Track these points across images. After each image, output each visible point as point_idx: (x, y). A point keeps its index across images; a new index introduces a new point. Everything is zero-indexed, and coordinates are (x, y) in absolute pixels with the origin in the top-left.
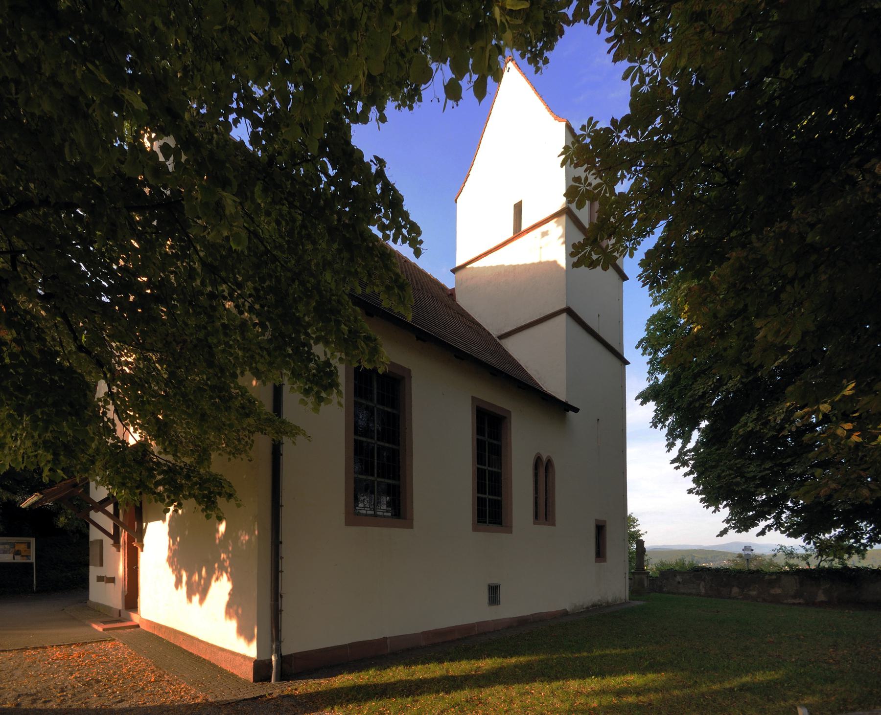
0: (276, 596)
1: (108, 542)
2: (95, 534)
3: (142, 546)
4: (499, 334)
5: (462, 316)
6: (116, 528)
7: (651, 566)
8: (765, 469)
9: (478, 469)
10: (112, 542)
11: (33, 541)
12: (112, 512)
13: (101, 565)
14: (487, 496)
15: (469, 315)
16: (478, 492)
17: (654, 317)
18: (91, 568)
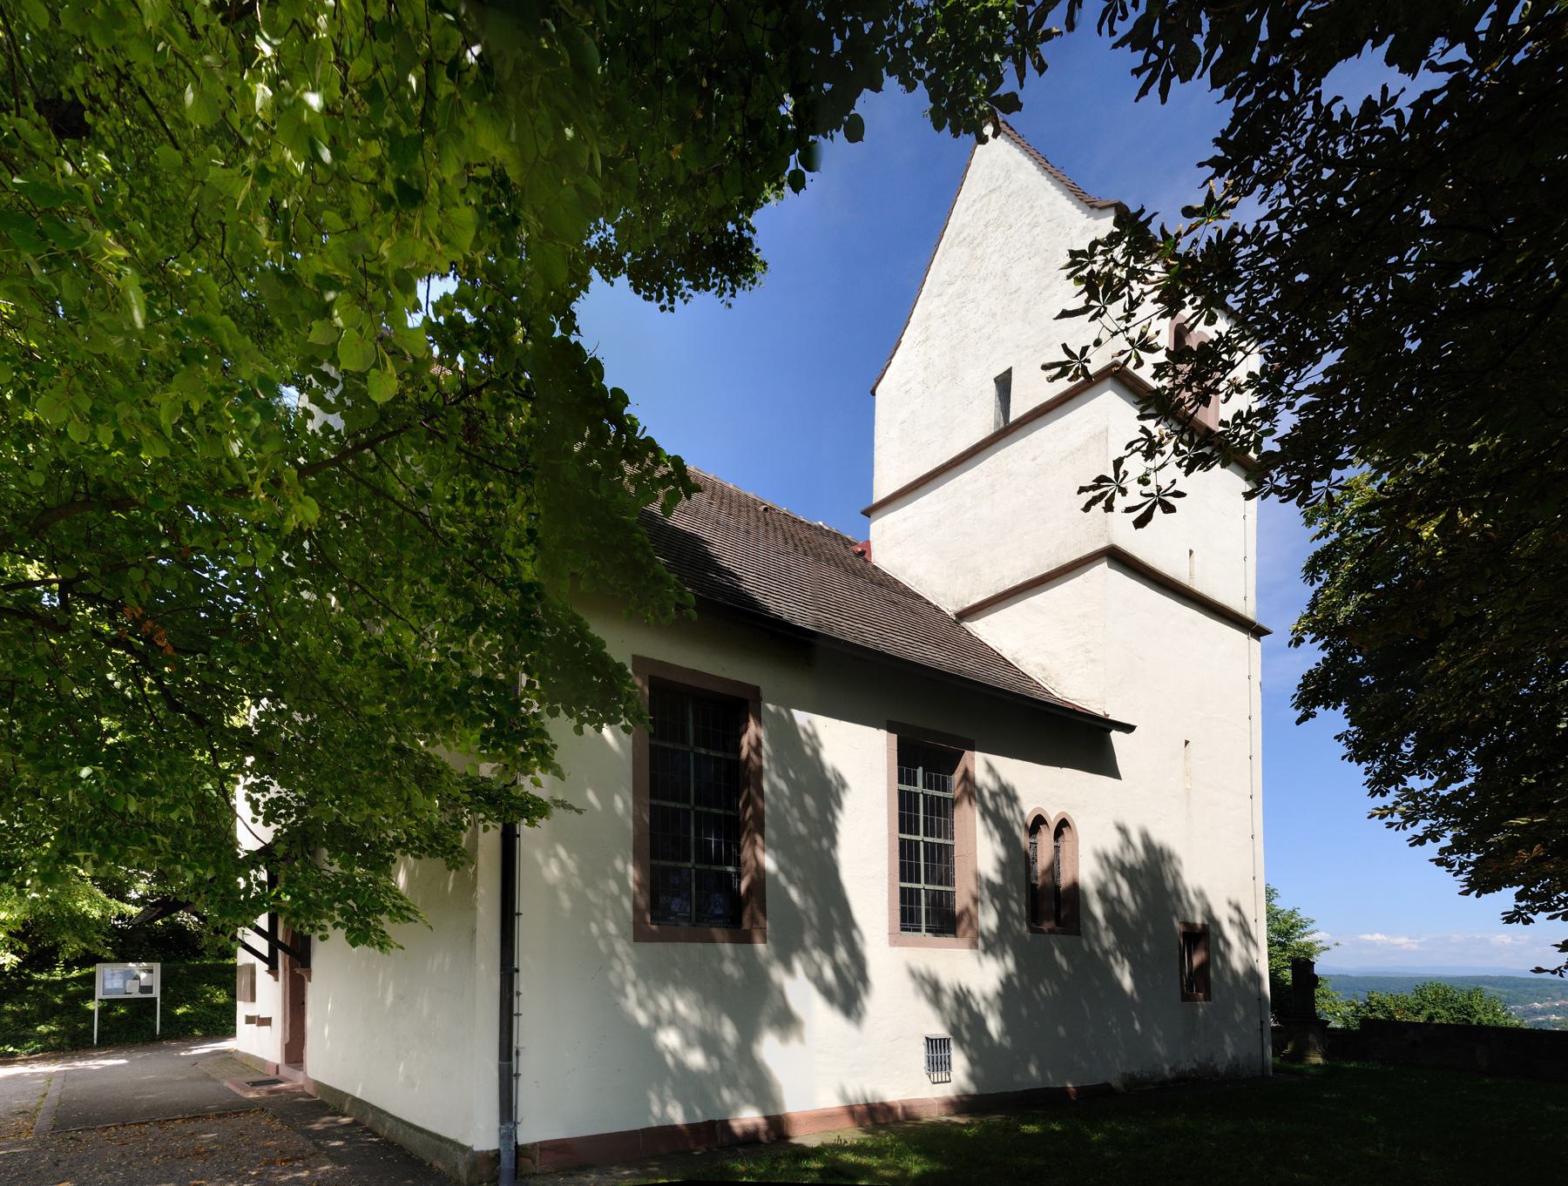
0: (507, 1051)
1: (262, 967)
2: (243, 958)
3: (309, 973)
4: (958, 609)
5: (880, 585)
6: (272, 950)
7: (1335, 1011)
8: (20, 1144)
9: (901, 792)
10: (266, 967)
11: (157, 967)
12: (266, 929)
13: (253, 999)
14: (919, 788)
15: (897, 582)
16: (902, 879)
17: (1317, 554)
18: (240, 1005)
